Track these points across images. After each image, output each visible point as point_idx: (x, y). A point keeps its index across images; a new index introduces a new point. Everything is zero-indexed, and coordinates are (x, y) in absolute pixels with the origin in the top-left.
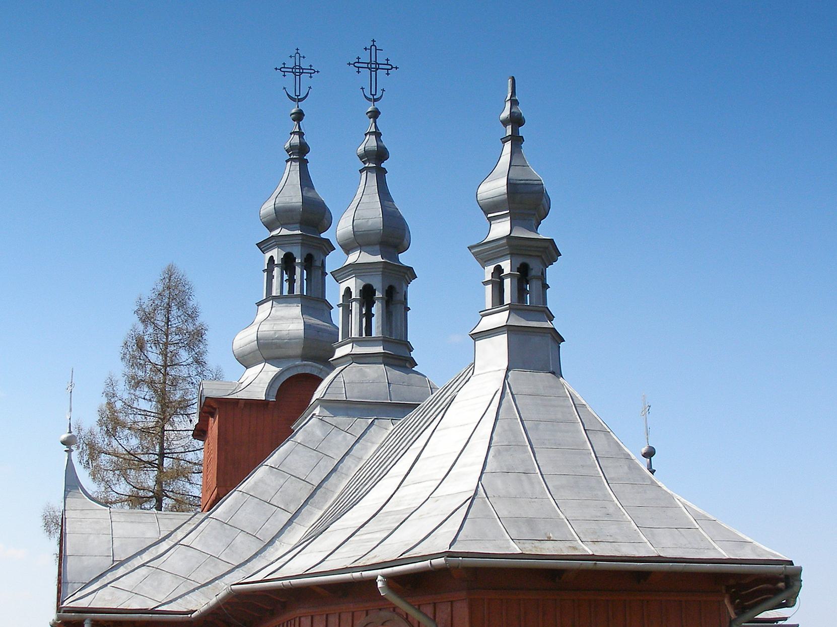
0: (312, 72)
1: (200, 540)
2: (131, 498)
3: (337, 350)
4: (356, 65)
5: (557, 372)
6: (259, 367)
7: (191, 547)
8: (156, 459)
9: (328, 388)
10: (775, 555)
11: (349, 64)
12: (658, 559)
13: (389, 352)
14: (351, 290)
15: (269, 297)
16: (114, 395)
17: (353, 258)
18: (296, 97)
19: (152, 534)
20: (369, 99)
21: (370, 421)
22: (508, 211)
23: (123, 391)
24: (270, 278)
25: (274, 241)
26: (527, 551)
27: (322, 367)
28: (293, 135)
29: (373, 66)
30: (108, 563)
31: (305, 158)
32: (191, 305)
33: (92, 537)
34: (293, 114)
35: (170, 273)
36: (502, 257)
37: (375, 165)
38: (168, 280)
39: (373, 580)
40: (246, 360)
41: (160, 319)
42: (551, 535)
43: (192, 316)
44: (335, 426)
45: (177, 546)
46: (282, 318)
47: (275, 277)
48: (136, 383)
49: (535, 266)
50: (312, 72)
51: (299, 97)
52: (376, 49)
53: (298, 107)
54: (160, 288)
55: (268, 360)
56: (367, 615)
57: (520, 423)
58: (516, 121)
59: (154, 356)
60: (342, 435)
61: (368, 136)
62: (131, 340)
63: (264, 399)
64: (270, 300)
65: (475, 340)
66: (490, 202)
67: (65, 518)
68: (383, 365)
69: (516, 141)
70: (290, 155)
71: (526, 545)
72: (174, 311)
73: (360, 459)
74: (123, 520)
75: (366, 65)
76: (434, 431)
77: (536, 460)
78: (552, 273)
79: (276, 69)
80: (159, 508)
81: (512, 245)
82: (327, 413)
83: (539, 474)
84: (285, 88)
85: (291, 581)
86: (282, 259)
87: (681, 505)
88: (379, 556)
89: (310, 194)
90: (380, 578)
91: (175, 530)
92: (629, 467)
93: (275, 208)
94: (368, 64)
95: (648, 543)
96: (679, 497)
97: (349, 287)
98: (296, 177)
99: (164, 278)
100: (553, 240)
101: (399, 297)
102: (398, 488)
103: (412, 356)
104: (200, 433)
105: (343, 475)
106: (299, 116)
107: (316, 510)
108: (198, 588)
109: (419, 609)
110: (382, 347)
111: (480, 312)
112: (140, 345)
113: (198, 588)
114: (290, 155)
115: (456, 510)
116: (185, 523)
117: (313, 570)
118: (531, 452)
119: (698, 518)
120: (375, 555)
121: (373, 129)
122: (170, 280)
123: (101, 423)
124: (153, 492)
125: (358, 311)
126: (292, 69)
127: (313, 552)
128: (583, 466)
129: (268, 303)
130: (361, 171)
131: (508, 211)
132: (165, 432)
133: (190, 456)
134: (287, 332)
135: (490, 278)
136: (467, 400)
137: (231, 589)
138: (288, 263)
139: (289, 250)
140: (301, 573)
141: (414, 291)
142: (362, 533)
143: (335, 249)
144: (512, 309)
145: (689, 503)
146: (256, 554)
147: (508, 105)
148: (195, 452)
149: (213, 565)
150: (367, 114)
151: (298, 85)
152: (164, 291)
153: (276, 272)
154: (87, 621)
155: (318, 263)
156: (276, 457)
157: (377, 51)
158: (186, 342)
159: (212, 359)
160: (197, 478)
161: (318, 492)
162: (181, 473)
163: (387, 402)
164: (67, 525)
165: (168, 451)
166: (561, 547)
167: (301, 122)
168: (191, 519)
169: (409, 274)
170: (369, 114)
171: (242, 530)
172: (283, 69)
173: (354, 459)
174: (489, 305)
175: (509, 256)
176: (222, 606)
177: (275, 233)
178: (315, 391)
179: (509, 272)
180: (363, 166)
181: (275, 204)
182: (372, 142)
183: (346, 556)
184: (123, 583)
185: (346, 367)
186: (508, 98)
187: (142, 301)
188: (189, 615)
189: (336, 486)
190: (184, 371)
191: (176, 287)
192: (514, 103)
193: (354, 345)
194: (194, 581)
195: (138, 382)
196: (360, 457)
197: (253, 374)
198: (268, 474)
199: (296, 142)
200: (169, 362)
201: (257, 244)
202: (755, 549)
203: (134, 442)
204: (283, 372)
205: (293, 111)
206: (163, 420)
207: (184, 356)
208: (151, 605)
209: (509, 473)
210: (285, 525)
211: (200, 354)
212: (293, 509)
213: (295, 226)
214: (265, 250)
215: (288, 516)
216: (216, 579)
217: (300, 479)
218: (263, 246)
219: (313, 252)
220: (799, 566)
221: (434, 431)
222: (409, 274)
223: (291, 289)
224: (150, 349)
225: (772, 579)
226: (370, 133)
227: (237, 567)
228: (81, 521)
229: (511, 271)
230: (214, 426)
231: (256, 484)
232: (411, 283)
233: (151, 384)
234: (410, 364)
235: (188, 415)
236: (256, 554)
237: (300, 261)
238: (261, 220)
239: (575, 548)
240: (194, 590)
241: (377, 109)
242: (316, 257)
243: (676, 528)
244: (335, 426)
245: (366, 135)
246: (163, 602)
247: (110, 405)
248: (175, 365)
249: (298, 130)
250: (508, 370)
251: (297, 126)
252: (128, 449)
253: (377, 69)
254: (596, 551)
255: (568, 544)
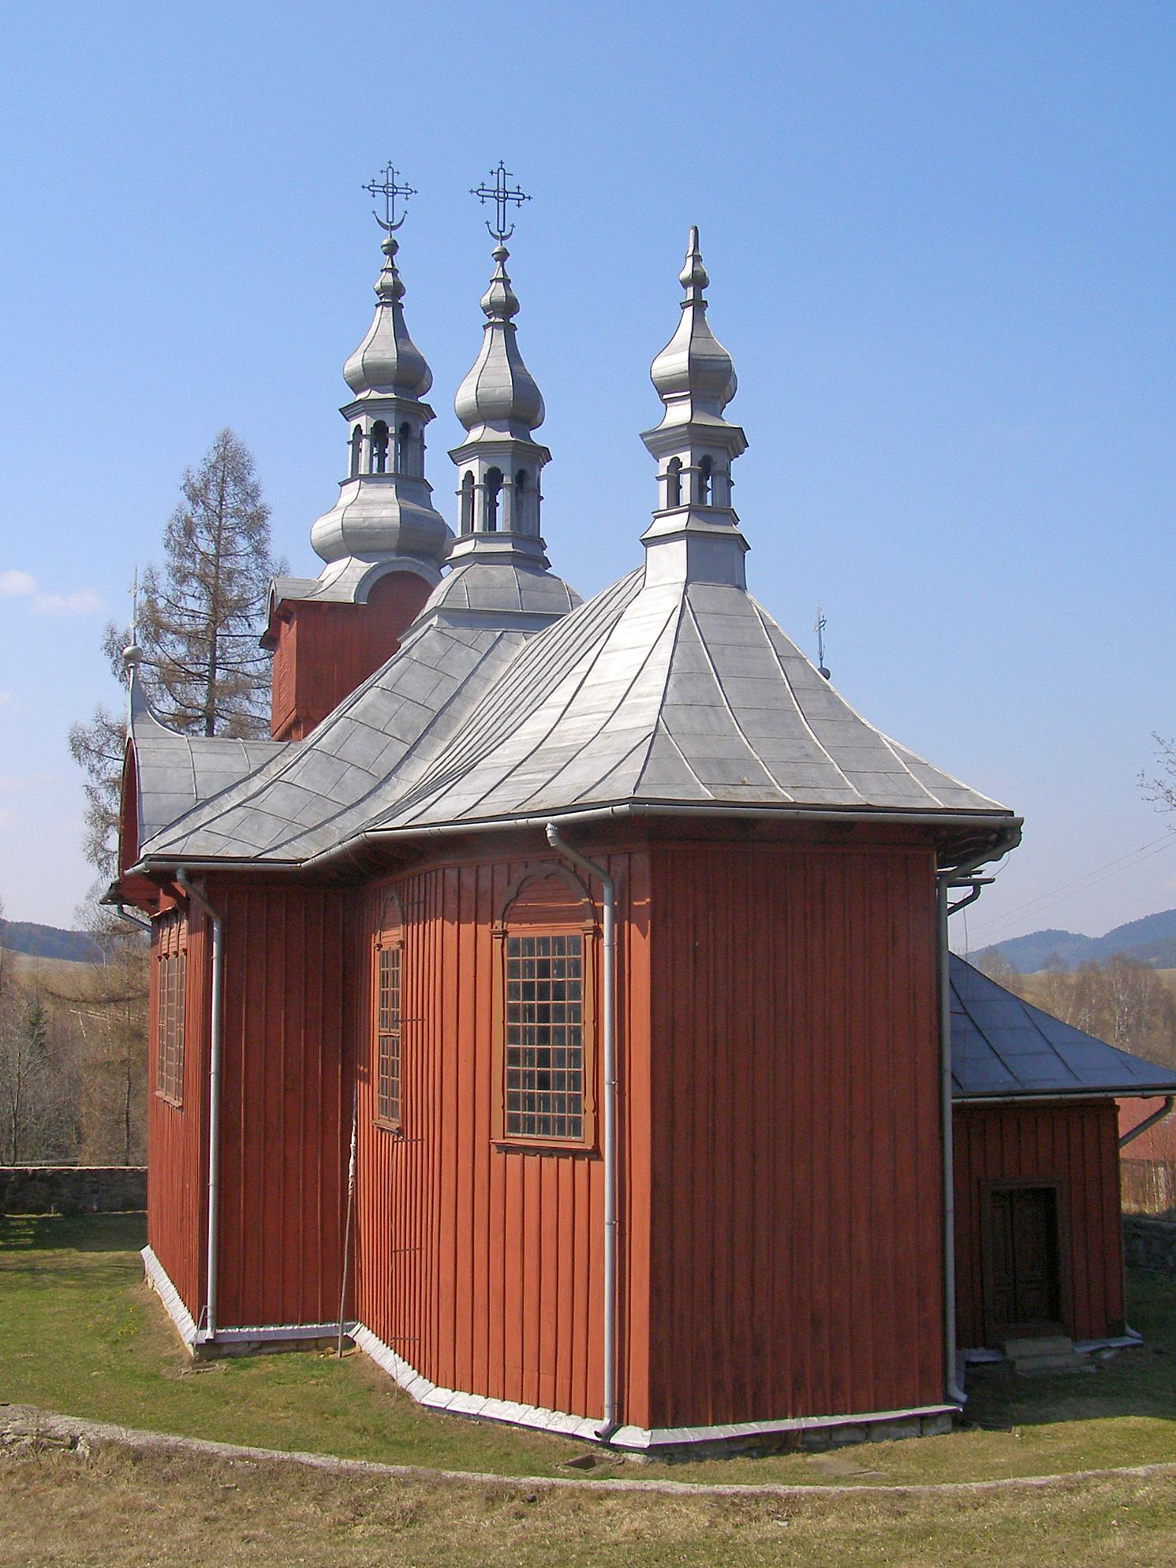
0: (410, 192)
1: (303, 775)
2: (176, 717)
3: (456, 547)
4: (479, 192)
5: (742, 587)
6: (344, 562)
7: (293, 784)
8: (207, 671)
9: (447, 593)
10: (996, 805)
11: (472, 192)
12: (866, 808)
13: (521, 551)
14: (474, 475)
15: (355, 476)
16: (155, 591)
17: (476, 434)
18: (389, 224)
19: (240, 768)
20: (496, 237)
21: (498, 634)
22: (689, 393)
23: (166, 584)
24: (357, 452)
25: (361, 406)
26: (721, 797)
27: (422, 563)
28: (384, 273)
29: (501, 195)
30: (190, 802)
31: (399, 301)
32: (252, 481)
33: (169, 771)
34: (384, 246)
35: (225, 439)
36: (681, 448)
37: (502, 320)
38: (223, 449)
39: (542, 828)
40: (328, 553)
41: (213, 498)
42: (745, 779)
43: (252, 495)
44: (457, 641)
45: (277, 783)
46: (372, 502)
47: (363, 451)
48: (181, 575)
49: (718, 457)
50: (410, 192)
51: (392, 225)
52: (505, 174)
53: (391, 237)
54: (213, 458)
55: (354, 553)
56: (526, 867)
57: (703, 647)
58: (698, 281)
59: (205, 544)
60: (465, 652)
61: (494, 283)
62: (176, 523)
63: (353, 601)
64: (356, 480)
65: (646, 546)
66: (667, 380)
67: (136, 749)
68: (512, 567)
69: (699, 306)
70: (381, 298)
71: (718, 791)
72: (230, 488)
73: (488, 680)
74: (204, 750)
75: (492, 194)
76: (599, 654)
77: (723, 691)
78: (738, 467)
79: (363, 187)
80: (210, 732)
81: (692, 434)
82: (446, 624)
83: (727, 707)
84: (374, 212)
85: (440, 828)
86: (372, 428)
87: (888, 746)
88: (546, 801)
89: (406, 349)
90: (549, 826)
91: (268, 763)
92: (829, 702)
93: (363, 365)
94: (494, 191)
95: (855, 790)
96: (886, 737)
97: (470, 471)
98: (388, 327)
99: (219, 446)
100: (741, 429)
101: (529, 484)
102: (559, 720)
103: (545, 555)
104: (269, 641)
105: (469, 699)
106: (392, 249)
107: (439, 741)
108: (306, 832)
109: (589, 859)
110: (511, 544)
111: (653, 513)
112: (189, 530)
113: (306, 832)
114: (381, 298)
115: (635, 748)
116: (279, 754)
117: (467, 816)
118: (717, 682)
119: (909, 760)
120: (540, 800)
121: (500, 275)
122: (225, 448)
123: (141, 624)
124: (204, 711)
125: (482, 499)
126: (384, 187)
127: (461, 794)
128: (776, 699)
129: (354, 483)
130: (485, 327)
131: (689, 393)
132: (217, 638)
133: (250, 668)
134: (379, 519)
135: (666, 473)
136: (639, 617)
137: (366, 836)
138: (379, 433)
139: (380, 418)
140: (452, 819)
141: (548, 477)
142: (521, 772)
143: (436, 417)
144: (692, 510)
145: (897, 744)
146: (370, 793)
147: (690, 261)
148: (255, 663)
149: (319, 805)
150: (493, 255)
151: (390, 209)
152: (218, 462)
153: (365, 444)
154: (179, 871)
155: (416, 435)
156: (389, 676)
157: (506, 176)
158: (243, 528)
159: (276, 549)
160: (258, 695)
161: (440, 719)
162: (241, 688)
163: (517, 611)
164: (139, 756)
165: (221, 661)
166: (759, 793)
167: (394, 257)
168: (284, 749)
169: (543, 455)
170: (495, 256)
171: (352, 765)
172: (372, 188)
173: (481, 680)
174: (663, 505)
175: (689, 446)
176: (350, 854)
177: (362, 396)
178: (429, 596)
179: (689, 466)
180: (487, 321)
181: (363, 361)
182: (499, 292)
183: (503, 800)
184: (219, 826)
185: (467, 569)
186: (690, 253)
187: (190, 474)
188: (299, 865)
189: (461, 712)
190: (242, 564)
191: (233, 458)
192: (697, 259)
193: (477, 542)
194: (300, 824)
195: (186, 576)
196: (487, 677)
197: (337, 571)
198: (379, 697)
199: (501, 295)
200: (224, 550)
201: (340, 410)
202: (972, 796)
203: (181, 650)
204: (376, 569)
205: (385, 242)
206: (215, 623)
207: (242, 544)
208: (253, 852)
209: (693, 707)
210: (403, 758)
211: (262, 541)
212: (411, 740)
213: (388, 387)
214: (350, 417)
215: (403, 749)
216: (326, 822)
217: (419, 704)
218: (348, 412)
219: (409, 420)
220: (1021, 816)
221: (599, 654)
222: (543, 455)
223: (381, 467)
224: (199, 535)
225: (987, 830)
226: (497, 280)
227: (349, 808)
228: (155, 752)
229: (691, 465)
230: (289, 634)
231: (366, 709)
232: (545, 466)
233: (202, 580)
234: (544, 565)
235: (246, 617)
236: (370, 793)
237: (394, 432)
238: (345, 379)
239: (773, 795)
240: (301, 835)
241: (395, 241)
242: (413, 426)
243: (885, 773)
244: (457, 641)
245: (492, 281)
246: (267, 849)
247: (151, 603)
248: (229, 555)
249: (502, 276)
250: (687, 583)
251: (390, 262)
252: (174, 657)
253: (506, 199)
254: (798, 798)
255: (766, 790)
